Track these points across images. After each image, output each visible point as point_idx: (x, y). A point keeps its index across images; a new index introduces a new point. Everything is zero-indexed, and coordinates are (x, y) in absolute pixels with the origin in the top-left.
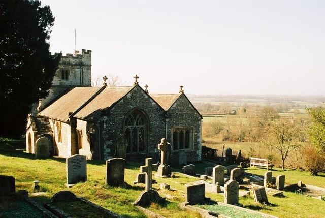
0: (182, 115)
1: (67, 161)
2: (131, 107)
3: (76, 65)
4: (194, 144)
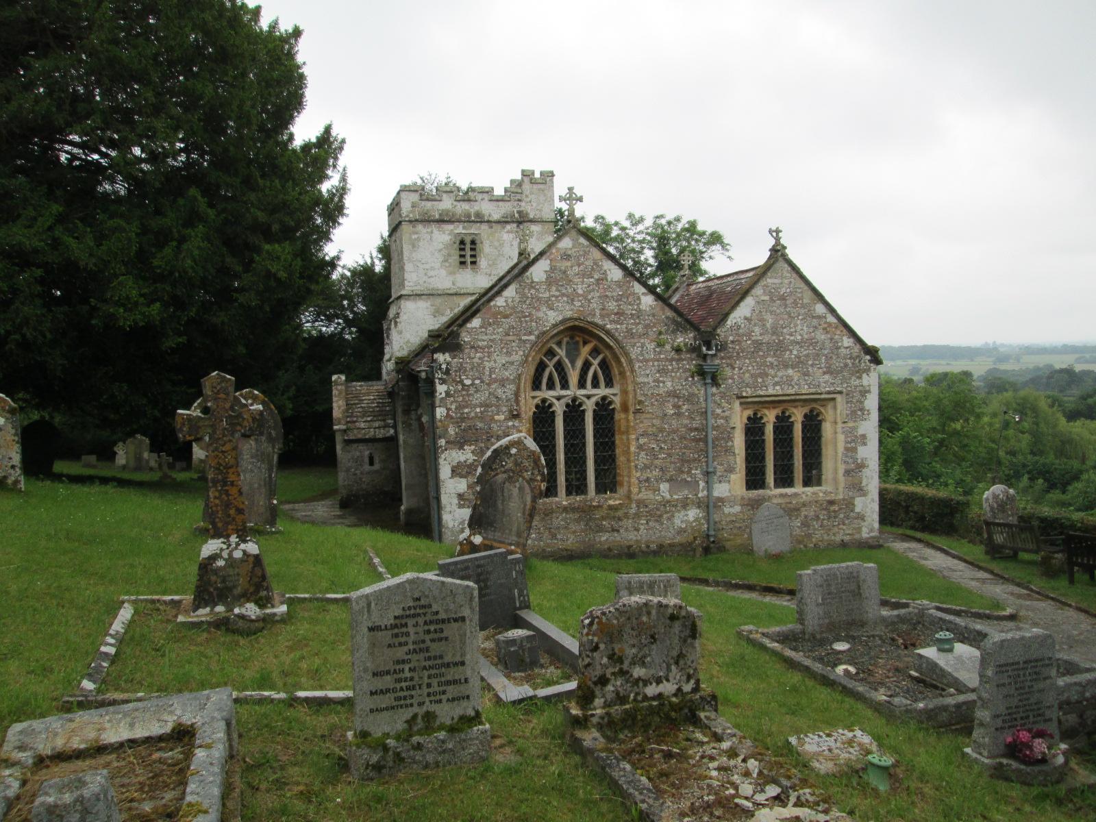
0: (780, 347)
1: (756, 492)
2: (551, 314)
3: (503, 222)
4: (841, 468)
